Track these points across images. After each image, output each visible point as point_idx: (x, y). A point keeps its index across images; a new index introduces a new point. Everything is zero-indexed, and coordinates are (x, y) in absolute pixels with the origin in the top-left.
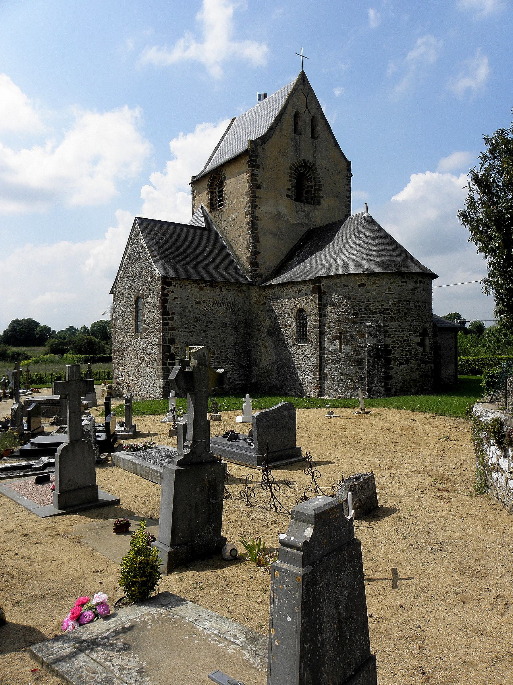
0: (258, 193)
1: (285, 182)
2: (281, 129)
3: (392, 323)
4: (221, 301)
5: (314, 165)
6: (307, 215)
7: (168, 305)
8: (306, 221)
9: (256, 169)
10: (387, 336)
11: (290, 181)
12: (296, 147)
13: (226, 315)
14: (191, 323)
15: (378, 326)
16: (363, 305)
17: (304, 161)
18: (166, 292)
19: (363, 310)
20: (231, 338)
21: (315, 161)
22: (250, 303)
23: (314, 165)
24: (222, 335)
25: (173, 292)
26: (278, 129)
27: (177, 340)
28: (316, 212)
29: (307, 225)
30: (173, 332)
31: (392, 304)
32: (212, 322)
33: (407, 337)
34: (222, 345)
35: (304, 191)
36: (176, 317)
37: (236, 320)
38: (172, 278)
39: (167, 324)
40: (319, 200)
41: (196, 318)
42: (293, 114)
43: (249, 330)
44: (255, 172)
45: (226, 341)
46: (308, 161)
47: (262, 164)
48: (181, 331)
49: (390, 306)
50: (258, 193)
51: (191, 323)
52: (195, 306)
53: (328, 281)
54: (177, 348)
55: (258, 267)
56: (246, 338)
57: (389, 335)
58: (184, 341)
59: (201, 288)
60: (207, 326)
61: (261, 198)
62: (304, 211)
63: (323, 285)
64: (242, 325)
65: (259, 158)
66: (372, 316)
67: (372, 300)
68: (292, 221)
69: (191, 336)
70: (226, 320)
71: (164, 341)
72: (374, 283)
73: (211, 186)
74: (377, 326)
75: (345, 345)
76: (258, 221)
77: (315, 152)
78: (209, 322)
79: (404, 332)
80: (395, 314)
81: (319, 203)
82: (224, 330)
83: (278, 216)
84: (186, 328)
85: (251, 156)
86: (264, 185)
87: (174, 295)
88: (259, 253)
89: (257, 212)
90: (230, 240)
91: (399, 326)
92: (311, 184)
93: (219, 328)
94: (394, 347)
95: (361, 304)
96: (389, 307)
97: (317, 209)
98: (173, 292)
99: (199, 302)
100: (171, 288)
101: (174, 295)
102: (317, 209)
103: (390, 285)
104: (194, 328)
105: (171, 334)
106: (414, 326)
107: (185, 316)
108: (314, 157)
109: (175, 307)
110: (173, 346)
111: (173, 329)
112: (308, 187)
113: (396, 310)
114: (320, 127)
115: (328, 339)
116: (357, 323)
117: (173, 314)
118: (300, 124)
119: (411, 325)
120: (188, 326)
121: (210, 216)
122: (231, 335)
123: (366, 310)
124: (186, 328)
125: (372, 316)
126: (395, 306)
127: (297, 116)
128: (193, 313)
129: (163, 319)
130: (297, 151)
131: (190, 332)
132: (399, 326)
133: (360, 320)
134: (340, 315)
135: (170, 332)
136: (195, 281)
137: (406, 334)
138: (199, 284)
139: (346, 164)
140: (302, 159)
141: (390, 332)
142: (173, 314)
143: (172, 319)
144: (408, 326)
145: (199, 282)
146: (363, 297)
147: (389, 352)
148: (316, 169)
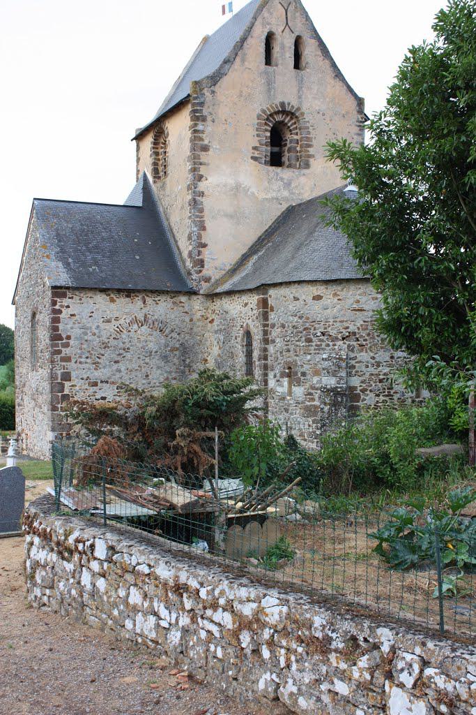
0: (204, 157)
1: (251, 137)
2: (243, 61)
3: (362, 354)
4: (143, 319)
5: (298, 109)
6: (288, 185)
7: (61, 326)
8: (286, 193)
9: (200, 123)
10: (353, 373)
11: (258, 136)
12: (269, 85)
13: (150, 338)
14: (96, 350)
15: (339, 358)
16: (320, 328)
17: (282, 104)
18: (57, 307)
19: (319, 334)
20: (159, 371)
21: (300, 103)
22: (191, 320)
23: (298, 109)
24: (144, 367)
25: (68, 307)
26: (238, 59)
27: (73, 375)
28: (303, 180)
29: (286, 199)
30: (68, 364)
31: (362, 325)
32: (128, 349)
33: (384, 374)
34: (144, 381)
35: (286, 148)
36: (71, 342)
37: (166, 346)
38: (68, 288)
39: (59, 352)
40: (308, 161)
41: (103, 344)
42: (264, 37)
43: (188, 361)
44: (200, 127)
45: (150, 377)
46: (289, 104)
47: (211, 114)
48: (80, 363)
49: (358, 328)
50: (204, 157)
51: (96, 350)
52: (103, 326)
53: (276, 291)
54: (73, 386)
55: (203, 266)
56: (183, 372)
57: (357, 372)
58: (85, 377)
59: (112, 301)
60: (120, 355)
61: (208, 164)
62: (282, 179)
63: (270, 296)
64: (177, 353)
65: (206, 106)
66: (331, 344)
67: (331, 320)
68: (262, 196)
69: (96, 369)
70: (152, 346)
71: (53, 377)
72: (335, 295)
73: (155, 144)
74: (336, 358)
75: (294, 385)
76: (203, 199)
77: (300, 89)
78: (124, 349)
79: (380, 368)
80: (365, 340)
81: (307, 166)
82: (147, 360)
83: (237, 189)
84: (87, 358)
85: (194, 105)
86: (215, 145)
87: (70, 311)
88: (205, 246)
89: (202, 186)
90: (172, 225)
91: (373, 358)
92: (295, 137)
93: (139, 358)
94: (363, 391)
95: (317, 326)
96: (357, 331)
97: (304, 175)
98: (68, 307)
99: (109, 321)
100: (66, 302)
101: (70, 311)
102: (304, 175)
103: (358, 297)
104: (99, 358)
105: (64, 367)
106: (398, 358)
107: (86, 341)
108: (300, 97)
109: (72, 328)
110: (67, 384)
111: (68, 359)
112: (291, 142)
113: (369, 335)
114: (309, 50)
115: (275, 376)
116: (310, 354)
117: (69, 337)
118: (276, 50)
119: (392, 357)
120: (91, 354)
121: (154, 187)
122: (158, 368)
123: (323, 334)
124: (87, 358)
125: (331, 344)
126: (367, 329)
127: (269, 39)
128: (99, 337)
129: (53, 346)
130: (269, 90)
131: (93, 364)
132: (373, 358)
133: (315, 350)
134: (289, 341)
135: (63, 363)
136: (103, 291)
137: (385, 371)
138: (109, 295)
139: (355, 103)
140: (277, 102)
141: (85, 384)
142: (69, 337)
143: (67, 345)
144: (388, 358)
145: (110, 292)
146: (319, 315)
147: (356, 398)
148: (303, 114)
